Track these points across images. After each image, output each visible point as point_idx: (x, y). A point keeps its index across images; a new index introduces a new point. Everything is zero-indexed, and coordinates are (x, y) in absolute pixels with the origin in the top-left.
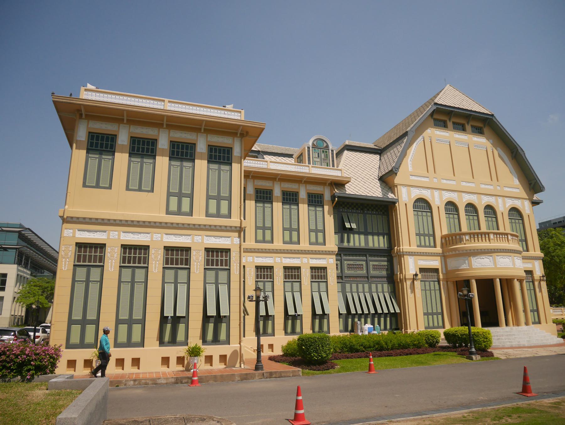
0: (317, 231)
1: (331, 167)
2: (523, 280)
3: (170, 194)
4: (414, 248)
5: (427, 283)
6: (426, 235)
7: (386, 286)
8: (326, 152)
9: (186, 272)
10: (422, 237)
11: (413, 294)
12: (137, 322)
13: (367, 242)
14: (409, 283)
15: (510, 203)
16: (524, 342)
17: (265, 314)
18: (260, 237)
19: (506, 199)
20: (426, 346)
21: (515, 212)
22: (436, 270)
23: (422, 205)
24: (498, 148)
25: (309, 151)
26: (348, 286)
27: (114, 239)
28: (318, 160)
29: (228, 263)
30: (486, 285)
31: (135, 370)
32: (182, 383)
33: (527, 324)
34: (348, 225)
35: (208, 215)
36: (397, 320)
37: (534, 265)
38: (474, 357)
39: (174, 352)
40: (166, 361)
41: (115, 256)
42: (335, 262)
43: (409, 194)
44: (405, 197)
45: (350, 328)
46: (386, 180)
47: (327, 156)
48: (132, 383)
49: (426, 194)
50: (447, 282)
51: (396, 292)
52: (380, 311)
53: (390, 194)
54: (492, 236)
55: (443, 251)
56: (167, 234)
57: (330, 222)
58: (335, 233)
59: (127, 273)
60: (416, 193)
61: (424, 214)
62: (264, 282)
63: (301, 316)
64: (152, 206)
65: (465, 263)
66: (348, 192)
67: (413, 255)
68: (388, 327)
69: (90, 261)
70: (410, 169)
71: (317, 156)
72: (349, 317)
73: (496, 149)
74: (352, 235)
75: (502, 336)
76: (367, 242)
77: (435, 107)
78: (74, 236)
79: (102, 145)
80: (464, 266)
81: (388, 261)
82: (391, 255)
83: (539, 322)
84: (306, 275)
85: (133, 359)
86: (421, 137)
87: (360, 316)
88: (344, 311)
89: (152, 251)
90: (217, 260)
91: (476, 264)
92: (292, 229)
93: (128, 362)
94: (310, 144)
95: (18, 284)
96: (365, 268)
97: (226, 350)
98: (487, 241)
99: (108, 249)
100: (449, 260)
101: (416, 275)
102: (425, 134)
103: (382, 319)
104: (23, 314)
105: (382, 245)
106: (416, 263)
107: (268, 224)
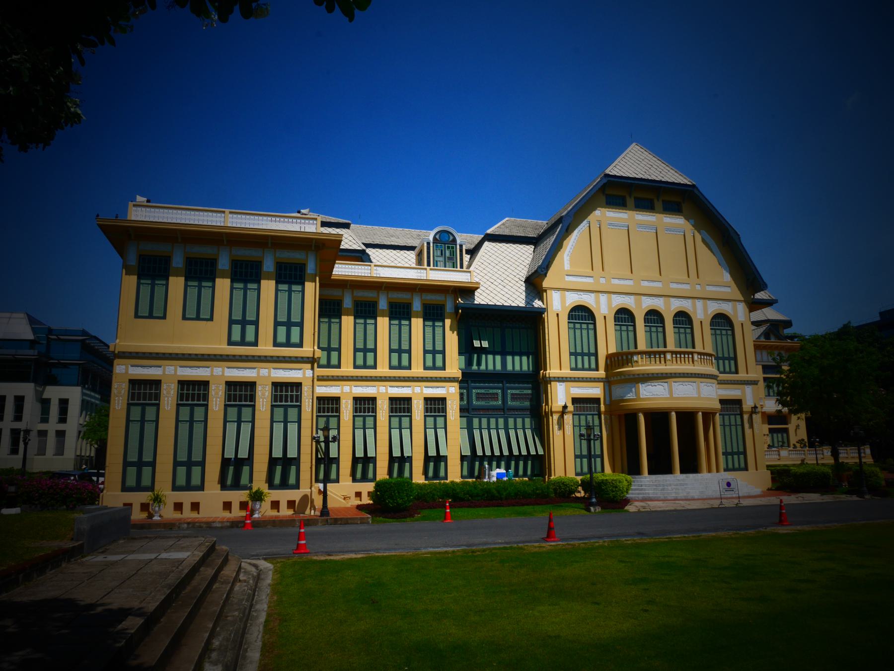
0: (435, 352)
1: (459, 269)
2: (714, 414)
3: (231, 322)
4: (566, 372)
5: (583, 417)
6: (583, 355)
7: (528, 421)
8: (453, 248)
9: (250, 409)
10: (579, 358)
11: (561, 432)
12: (197, 464)
13: (504, 363)
14: (556, 417)
15: (714, 308)
16: (695, 494)
17: (362, 455)
18: (360, 362)
19: (709, 302)
20: (562, 494)
21: (721, 321)
22: (596, 401)
23: (581, 315)
24: (703, 232)
25: (428, 248)
26: (476, 421)
27: (171, 374)
28: (442, 259)
29: (299, 398)
30: (658, 418)
31: (194, 515)
32: (237, 527)
33: (710, 471)
34: (477, 344)
35: (276, 344)
36: (541, 464)
37: (744, 392)
38: (592, 509)
39: (237, 497)
40: (227, 506)
41: (172, 392)
42: (458, 391)
43: (563, 300)
44: (557, 303)
45: (476, 473)
46: (534, 284)
47: (453, 253)
48: (186, 525)
49: (588, 300)
50: (611, 415)
51: (541, 431)
52: (516, 452)
53: (536, 301)
54: (669, 356)
55: (607, 375)
56: (228, 368)
57: (452, 340)
58: (460, 353)
59: (185, 412)
60: (573, 299)
61: (584, 326)
62: (364, 417)
63: (445, 458)
64: (212, 337)
65: (631, 391)
66: (478, 301)
67: (563, 381)
68: (529, 472)
69: (144, 400)
70: (567, 266)
71: (439, 253)
72: (473, 461)
73: (699, 232)
74: (484, 356)
75: (670, 485)
76: (504, 363)
77: (605, 181)
78: (127, 372)
79: (153, 270)
80: (630, 396)
81: (532, 389)
82: (537, 383)
83: (746, 469)
84: (418, 409)
85: (192, 504)
86: (585, 222)
87: (492, 458)
88: (467, 452)
89: (212, 387)
90: (286, 396)
91: (645, 393)
92: (401, 352)
93: (187, 507)
94: (431, 239)
95: (84, 413)
96: (500, 398)
97: (295, 495)
98: (663, 362)
99: (164, 386)
100: (613, 387)
101: (565, 407)
102: (590, 218)
103: (521, 463)
104: (93, 454)
105: (525, 368)
106: (567, 391)
107: (370, 345)
